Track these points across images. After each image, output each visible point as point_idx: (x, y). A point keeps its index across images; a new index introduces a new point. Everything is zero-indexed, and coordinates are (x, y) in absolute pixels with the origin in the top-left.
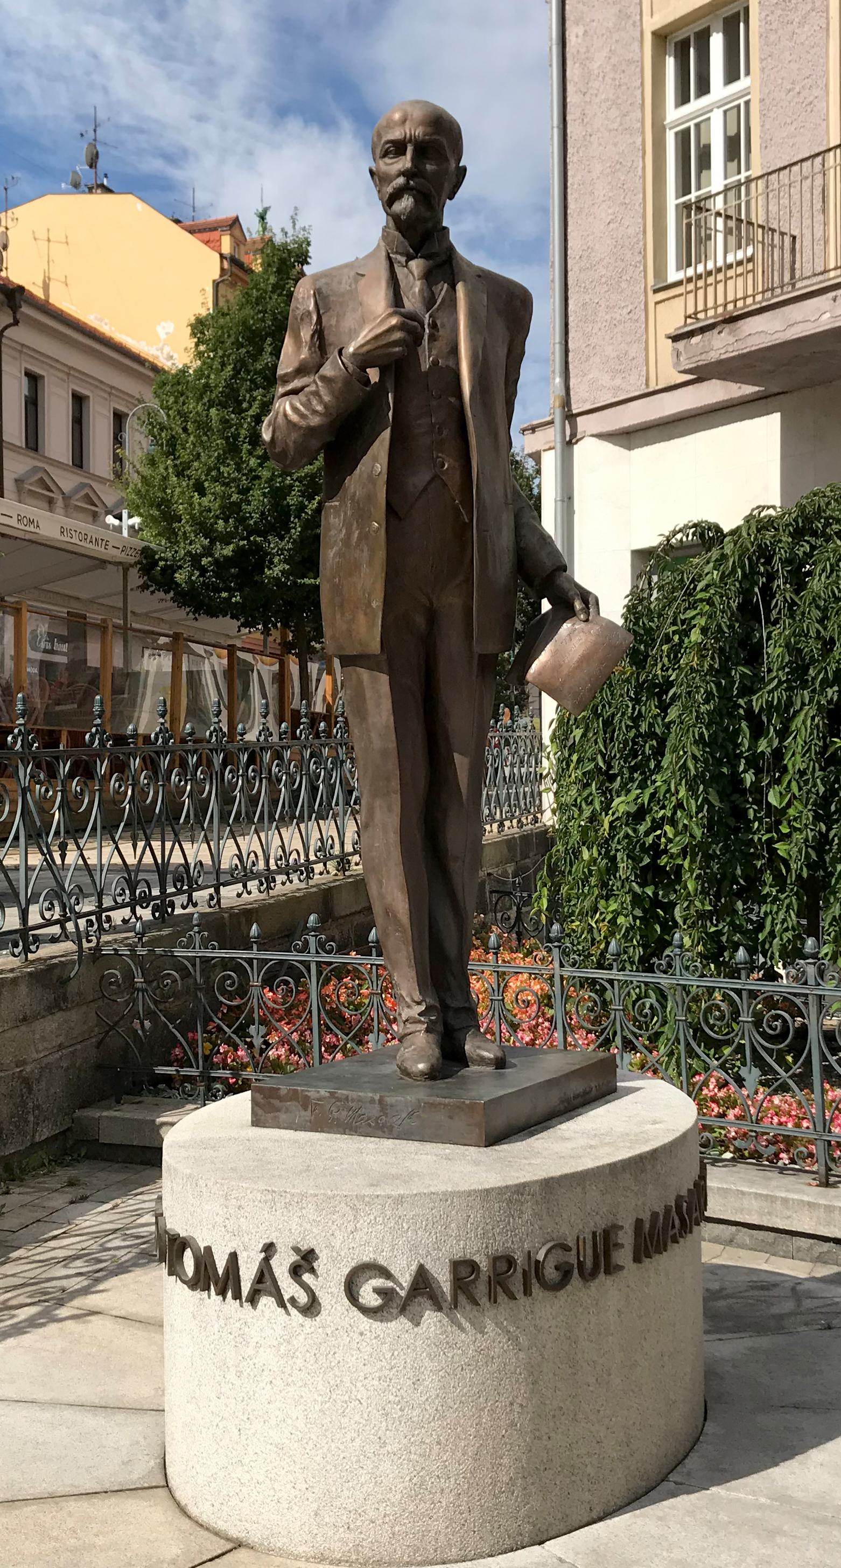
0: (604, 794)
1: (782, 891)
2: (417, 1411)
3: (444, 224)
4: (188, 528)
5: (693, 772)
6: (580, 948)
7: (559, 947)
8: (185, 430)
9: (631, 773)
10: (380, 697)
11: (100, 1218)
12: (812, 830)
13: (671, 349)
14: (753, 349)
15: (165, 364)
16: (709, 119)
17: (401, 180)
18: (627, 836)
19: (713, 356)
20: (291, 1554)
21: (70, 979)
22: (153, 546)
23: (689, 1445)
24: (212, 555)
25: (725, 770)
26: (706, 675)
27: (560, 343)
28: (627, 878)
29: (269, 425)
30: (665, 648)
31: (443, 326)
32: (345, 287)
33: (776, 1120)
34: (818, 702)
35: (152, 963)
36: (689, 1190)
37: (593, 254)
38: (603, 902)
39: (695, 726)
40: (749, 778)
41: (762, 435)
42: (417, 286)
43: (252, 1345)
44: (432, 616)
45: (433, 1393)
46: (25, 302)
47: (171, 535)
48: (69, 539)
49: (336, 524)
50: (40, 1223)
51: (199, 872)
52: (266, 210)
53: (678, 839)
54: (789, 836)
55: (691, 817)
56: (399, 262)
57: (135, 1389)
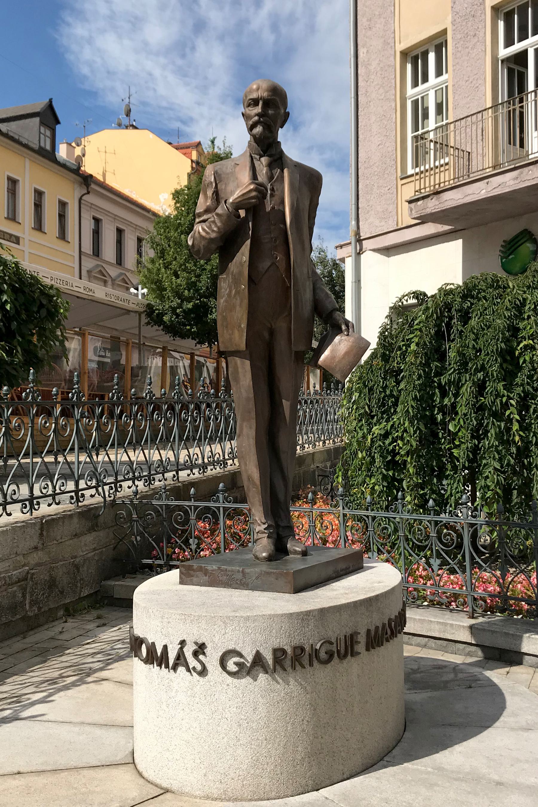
0: (369, 425)
1: (456, 473)
2: (256, 723)
3: (278, 140)
4: (170, 294)
5: (412, 414)
6: (358, 502)
7: (343, 499)
8: (169, 246)
9: (382, 415)
10: (246, 371)
11: (112, 634)
12: (470, 443)
13: (408, 207)
14: (448, 207)
15: (161, 213)
16: (428, 94)
17: (256, 118)
18: (380, 446)
19: (428, 211)
20: (193, 795)
21: (99, 515)
22: (152, 303)
23: (394, 744)
24: (182, 308)
25: (427, 413)
26: (418, 366)
27: (355, 204)
28: (380, 467)
29: (191, 237)
30: (398, 353)
31: (277, 190)
32: (229, 170)
33: (451, 586)
34: (473, 380)
35: (141, 508)
36: (396, 616)
37: (371, 161)
38: (368, 479)
39: (412, 391)
40: (439, 417)
41: (454, 249)
42: (265, 170)
43: (174, 691)
44: (272, 332)
45: (263, 715)
46: (93, 182)
47: (162, 298)
48: (110, 299)
49: (224, 285)
50: (81, 637)
51: (168, 463)
52: (214, 139)
53: (404, 447)
54: (459, 446)
55: (411, 437)
56: (256, 158)
57: (121, 717)
